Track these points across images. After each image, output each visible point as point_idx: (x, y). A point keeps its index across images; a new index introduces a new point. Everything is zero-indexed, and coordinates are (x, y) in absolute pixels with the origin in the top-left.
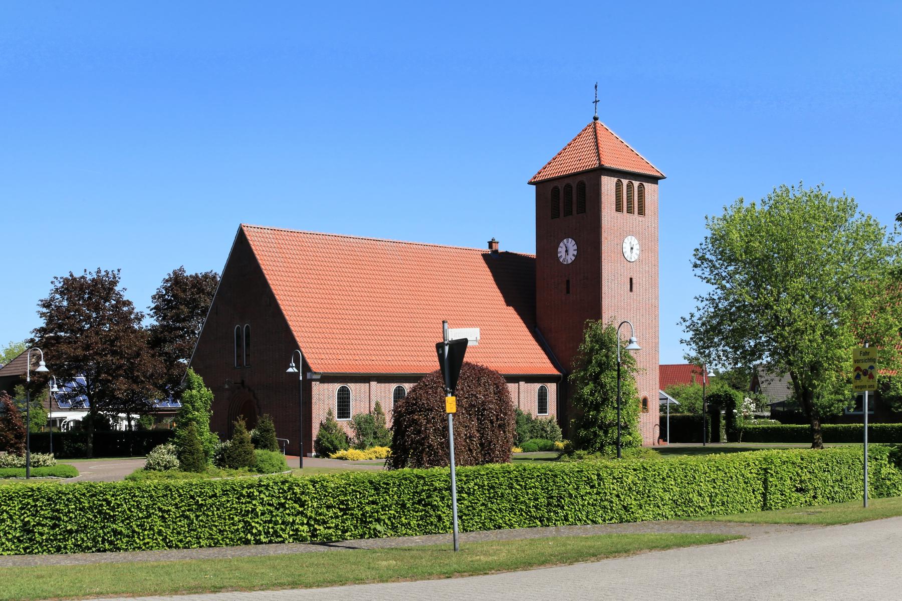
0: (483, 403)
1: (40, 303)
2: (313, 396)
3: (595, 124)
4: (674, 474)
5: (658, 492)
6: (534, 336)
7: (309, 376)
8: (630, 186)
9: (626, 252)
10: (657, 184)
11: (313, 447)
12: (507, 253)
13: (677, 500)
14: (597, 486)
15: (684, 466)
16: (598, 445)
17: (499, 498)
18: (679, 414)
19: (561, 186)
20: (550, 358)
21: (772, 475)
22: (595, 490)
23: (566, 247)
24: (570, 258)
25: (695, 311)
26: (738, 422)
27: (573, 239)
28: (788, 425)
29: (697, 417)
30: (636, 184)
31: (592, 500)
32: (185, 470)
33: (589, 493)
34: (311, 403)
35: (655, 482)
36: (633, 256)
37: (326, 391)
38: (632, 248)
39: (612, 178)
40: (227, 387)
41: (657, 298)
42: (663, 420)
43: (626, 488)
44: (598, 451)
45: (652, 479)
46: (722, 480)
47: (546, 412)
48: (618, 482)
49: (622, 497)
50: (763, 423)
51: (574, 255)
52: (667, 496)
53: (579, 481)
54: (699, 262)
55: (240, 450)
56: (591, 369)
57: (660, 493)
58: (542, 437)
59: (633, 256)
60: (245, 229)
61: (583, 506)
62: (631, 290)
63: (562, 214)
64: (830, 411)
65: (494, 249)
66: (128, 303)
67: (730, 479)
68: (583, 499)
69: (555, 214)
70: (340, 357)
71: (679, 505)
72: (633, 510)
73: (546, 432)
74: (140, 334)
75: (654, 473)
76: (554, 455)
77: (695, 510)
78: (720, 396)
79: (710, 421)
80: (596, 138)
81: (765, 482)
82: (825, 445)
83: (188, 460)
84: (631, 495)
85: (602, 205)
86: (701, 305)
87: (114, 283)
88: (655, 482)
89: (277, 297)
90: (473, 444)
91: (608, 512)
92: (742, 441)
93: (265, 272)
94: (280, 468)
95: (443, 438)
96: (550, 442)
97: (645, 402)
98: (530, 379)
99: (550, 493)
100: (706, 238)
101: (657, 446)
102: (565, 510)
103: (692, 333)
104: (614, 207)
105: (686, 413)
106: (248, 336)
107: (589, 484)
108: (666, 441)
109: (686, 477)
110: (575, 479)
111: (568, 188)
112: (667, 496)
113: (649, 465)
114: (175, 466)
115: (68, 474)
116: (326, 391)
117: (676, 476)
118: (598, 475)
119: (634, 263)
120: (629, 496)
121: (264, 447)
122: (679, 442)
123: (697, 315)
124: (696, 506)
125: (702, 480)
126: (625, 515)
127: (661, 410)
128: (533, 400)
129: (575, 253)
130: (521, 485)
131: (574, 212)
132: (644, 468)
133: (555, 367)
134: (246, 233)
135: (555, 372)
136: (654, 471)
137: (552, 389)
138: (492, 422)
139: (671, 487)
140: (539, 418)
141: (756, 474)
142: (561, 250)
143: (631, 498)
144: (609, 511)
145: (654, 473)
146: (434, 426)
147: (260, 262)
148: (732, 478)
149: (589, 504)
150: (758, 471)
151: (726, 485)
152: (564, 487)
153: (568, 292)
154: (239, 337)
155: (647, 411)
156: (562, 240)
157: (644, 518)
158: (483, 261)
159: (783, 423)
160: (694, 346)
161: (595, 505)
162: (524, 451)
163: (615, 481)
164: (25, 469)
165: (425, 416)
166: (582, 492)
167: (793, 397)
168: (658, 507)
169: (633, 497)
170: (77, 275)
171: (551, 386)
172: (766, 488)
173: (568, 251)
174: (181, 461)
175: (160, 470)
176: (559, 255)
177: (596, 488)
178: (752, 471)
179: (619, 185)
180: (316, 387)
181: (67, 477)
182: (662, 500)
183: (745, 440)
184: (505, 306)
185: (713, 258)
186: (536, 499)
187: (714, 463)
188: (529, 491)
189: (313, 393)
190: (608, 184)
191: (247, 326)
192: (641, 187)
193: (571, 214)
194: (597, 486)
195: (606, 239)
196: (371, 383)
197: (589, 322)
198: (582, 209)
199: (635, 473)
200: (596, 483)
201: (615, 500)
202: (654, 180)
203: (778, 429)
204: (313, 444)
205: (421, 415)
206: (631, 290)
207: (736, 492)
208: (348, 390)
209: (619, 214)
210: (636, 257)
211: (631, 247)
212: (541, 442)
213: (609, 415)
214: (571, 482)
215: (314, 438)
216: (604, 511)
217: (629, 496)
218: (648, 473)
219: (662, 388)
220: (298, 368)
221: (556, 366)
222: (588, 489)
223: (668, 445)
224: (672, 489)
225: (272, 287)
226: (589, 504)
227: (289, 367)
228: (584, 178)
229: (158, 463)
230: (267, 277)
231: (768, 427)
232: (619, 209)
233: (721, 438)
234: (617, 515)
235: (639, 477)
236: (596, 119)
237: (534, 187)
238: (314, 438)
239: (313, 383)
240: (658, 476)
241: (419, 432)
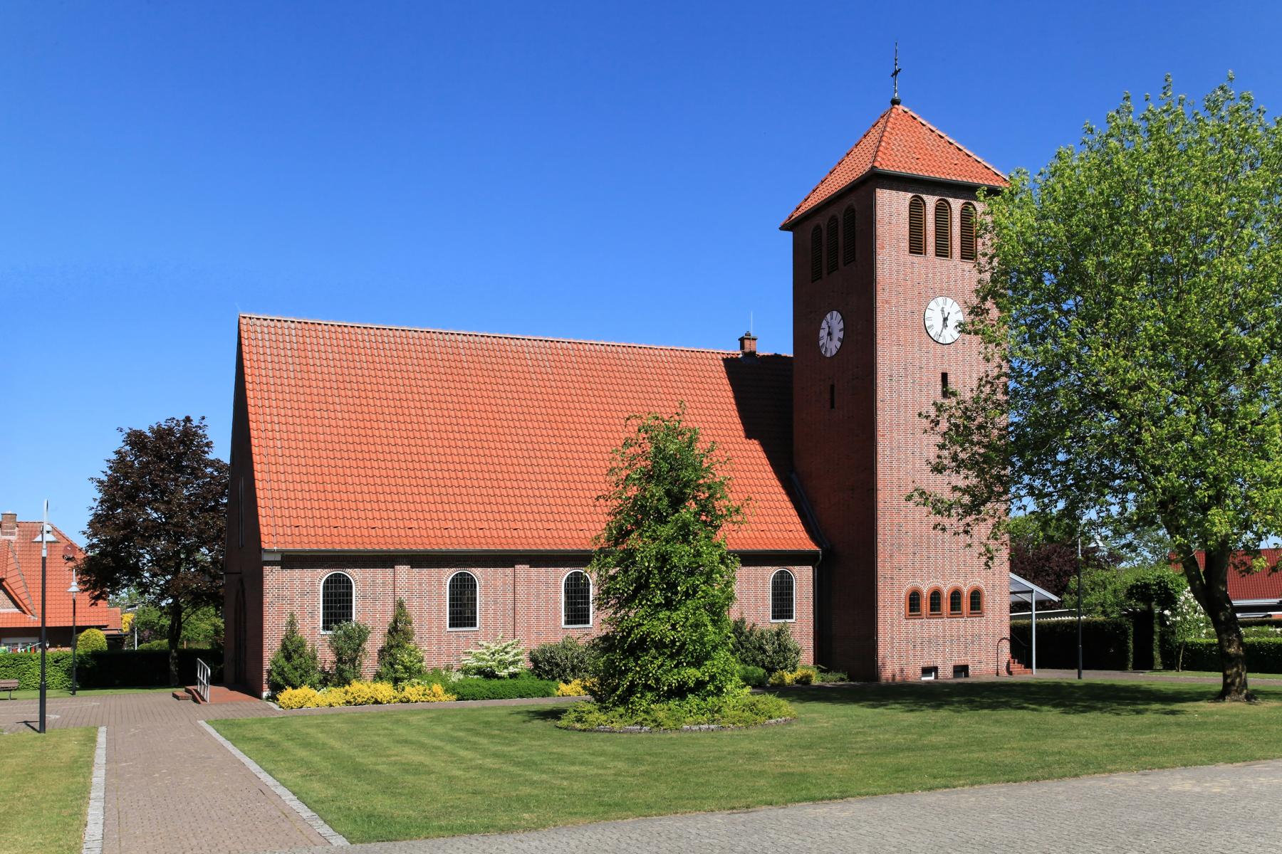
6: (784, 487)
8: (942, 210)
9: (931, 326)
11: (265, 681)
19: (822, 221)
23: (829, 327)
27: (838, 311)
29: (1109, 623)
37: (297, 583)
38: (945, 319)
39: (902, 193)
47: (791, 617)
50: (1257, 634)
63: (825, 272)
65: (747, 350)
69: (817, 276)
78: (1147, 586)
79: (1131, 631)
85: (878, 242)
92: (1183, 669)
104: (905, 245)
108: (1031, 667)
116: (297, 583)
128: (760, 594)
135: (809, 546)
137: (803, 577)
155: (981, 615)
171: (800, 572)
179: (916, 208)
180: (274, 578)
195: (887, 302)
196: (517, 567)
208: (348, 581)
209: (916, 259)
221: (813, 535)
223: (1036, 675)
232: (916, 247)
237: (790, 234)
238: (267, 665)
239: (267, 569)
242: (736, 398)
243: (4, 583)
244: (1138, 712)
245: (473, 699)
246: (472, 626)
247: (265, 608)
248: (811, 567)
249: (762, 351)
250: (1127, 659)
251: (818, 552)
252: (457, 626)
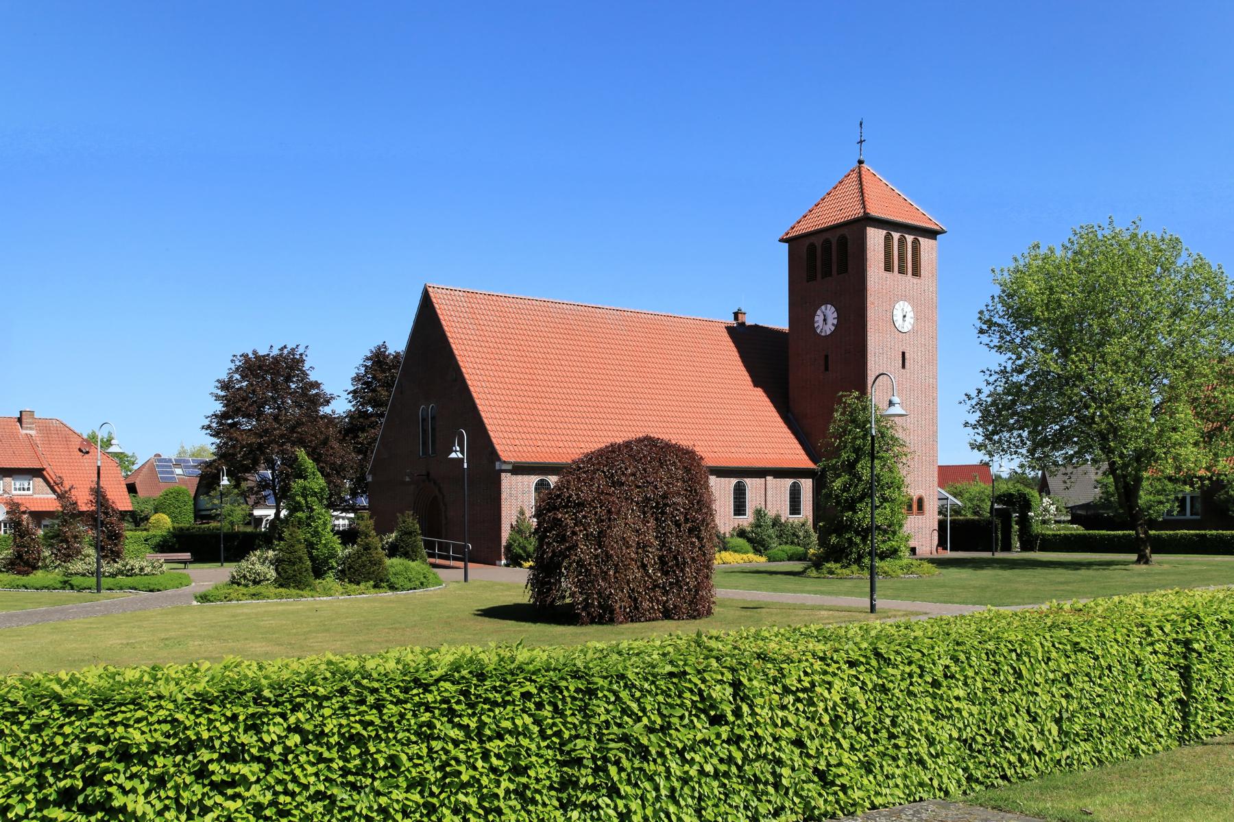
0: (665, 496)
1: (217, 384)
3: (859, 168)
4: (963, 670)
5: (919, 722)
8: (902, 241)
12: (756, 326)
13: (973, 739)
14: (731, 718)
15: (991, 646)
16: (854, 556)
17: (382, 774)
18: (961, 518)
19: (818, 242)
20: (804, 449)
21: (1200, 654)
22: (724, 731)
24: (829, 329)
25: (983, 386)
26: (1034, 526)
28: (1097, 532)
30: (910, 238)
31: (715, 761)
32: (281, 586)
33: (706, 742)
35: (911, 694)
36: (907, 326)
37: (520, 485)
38: (904, 316)
40: (408, 479)
41: (935, 377)
42: (942, 525)
43: (826, 719)
44: (854, 563)
45: (904, 685)
46: (1088, 675)
47: (799, 514)
48: (798, 700)
49: (812, 746)
50: (1064, 529)
52: (944, 732)
53: (672, 706)
54: (985, 327)
55: (364, 558)
56: (844, 456)
57: (925, 724)
58: (792, 543)
59: (907, 326)
60: (430, 290)
61: (685, 780)
62: (903, 366)
63: (819, 276)
64: (1149, 514)
66: (316, 385)
67: (1106, 672)
68: (684, 761)
69: (811, 277)
70: (539, 443)
71: (979, 752)
72: (845, 781)
73: (798, 537)
74: (329, 420)
75: (907, 669)
76: (797, 566)
77: (1020, 760)
78: (1011, 495)
79: (1000, 526)
80: (861, 184)
81: (1185, 674)
82: (1155, 557)
83: (286, 572)
84: (838, 736)
86: (991, 379)
88: (911, 694)
89: (464, 370)
90: (648, 556)
91: (767, 793)
93: (451, 340)
94: (422, 584)
95: (600, 548)
96: (801, 549)
97: (920, 501)
98: (780, 473)
99: (566, 748)
100: (993, 297)
101: (935, 556)
102: (621, 797)
103: (978, 414)
104: (882, 265)
105: (970, 516)
107: (704, 711)
108: (946, 549)
109: (996, 673)
110: (661, 698)
111: (827, 243)
112: (944, 732)
113: (893, 647)
114: (268, 580)
115: (151, 587)
116: (520, 485)
117: (970, 673)
118: (736, 685)
120: (833, 739)
121: (406, 555)
122: (962, 550)
123: (987, 390)
124: (1023, 749)
125: (1040, 680)
126: (820, 795)
127: (940, 513)
129: (835, 322)
130: (465, 728)
132: (878, 655)
134: (431, 294)
135: (809, 465)
136: (910, 663)
137: (807, 485)
138: (678, 525)
139: (956, 704)
140: (791, 520)
141: (1165, 654)
142: (819, 319)
143: (839, 745)
144: (771, 789)
145: (907, 669)
146: (585, 529)
147: (446, 328)
148: (1109, 668)
149: (702, 772)
150: (1170, 648)
151: (1097, 689)
152: (619, 726)
153: (827, 369)
154: (423, 420)
156: (819, 307)
157: (878, 801)
158: (726, 334)
159: (1087, 529)
160: (980, 430)
161: (726, 775)
162: (770, 560)
163: (791, 698)
165: (574, 514)
166: (681, 737)
167: (1101, 498)
168: (921, 762)
169: (846, 744)
170: (262, 352)
172: (1188, 690)
173: (826, 320)
174: (278, 573)
175: (246, 586)
176: (816, 325)
177: (727, 723)
178: (1157, 646)
179: (888, 239)
180: (507, 481)
181: (151, 591)
182: (931, 742)
183: (1043, 548)
184: (752, 387)
185: (1004, 321)
186: (518, 771)
187: (1067, 632)
188: (494, 746)
189: (503, 487)
190: (875, 237)
192: (916, 242)
193: (831, 275)
194: (731, 718)
197: (843, 396)
198: (843, 268)
199: (853, 672)
200: (728, 710)
201: (789, 753)
202: (932, 234)
203: (1084, 535)
204: (503, 550)
205: (567, 512)
206: (903, 366)
207: (1121, 704)
209: (888, 274)
210: (910, 327)
211: (904, 314)
212: (789, 548)
213: (863, 515)
214: (643, 710)
215: (504, 543)
216: (754, 793)
217: (833, 739)
218: (890, 670)
219: (941, 485)
220: (462, 453)
222: (703, 729)
223: (949, 554)
224: (958, 710)
225: (458, 358)
226: (702, 772)
227: (453, 451)
228: (845, 231)
229: (245, 577)
230: (453, 346)
231: (1072, 534)
232: (888, 267)
233: (1013, 546)
234: (797, 800)
235: (863, 683)
236: (860, 162)
237: (786, 246)
238: (504, 543)
240: (921, 676)
241: (562, 539)
242: (741, 357)
243: (45, 473)
247: (503, 503)
249: (748, 323)
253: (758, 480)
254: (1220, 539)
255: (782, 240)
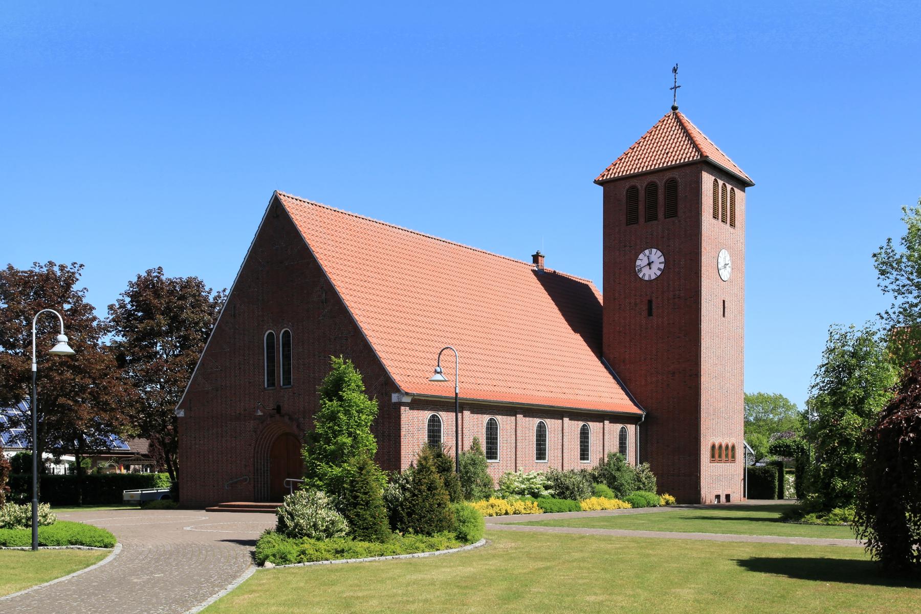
2: (402, 426)
7: (395, 398)
10: (744, 191)
19: (641, 185)
27: (658, 249)
34: (400, 436)
51: (659, 269)
63: (642, 220)
69: (632, 219)
87: (70, 280)
106: (286, 344)
119: (727, 282)
131: (661, 215)
133: (635, 404)
135: (634, 410)
137: (631, 429)
142: (642, 261)
153: (650, 313)
154: (271, 346)
156: (642, 251)
164: (30, 530)
174: (351, 522)
190: (707, 180)
191: (286, 331)
193: (656, 219)
198: (672, 211)
223: (677, 505)
228: (675, 174)
229: (315, 526)
232: (715, 217)
239: (402, 408)
244: (432, 547)
245: (551, 512)
246: (495, 459)
248: (634, 426)
250: (774, 492)
251: (641, 415)
252: (540, 460)
253: (598, 423)
254: (245, 510)
255: (597, 182)
